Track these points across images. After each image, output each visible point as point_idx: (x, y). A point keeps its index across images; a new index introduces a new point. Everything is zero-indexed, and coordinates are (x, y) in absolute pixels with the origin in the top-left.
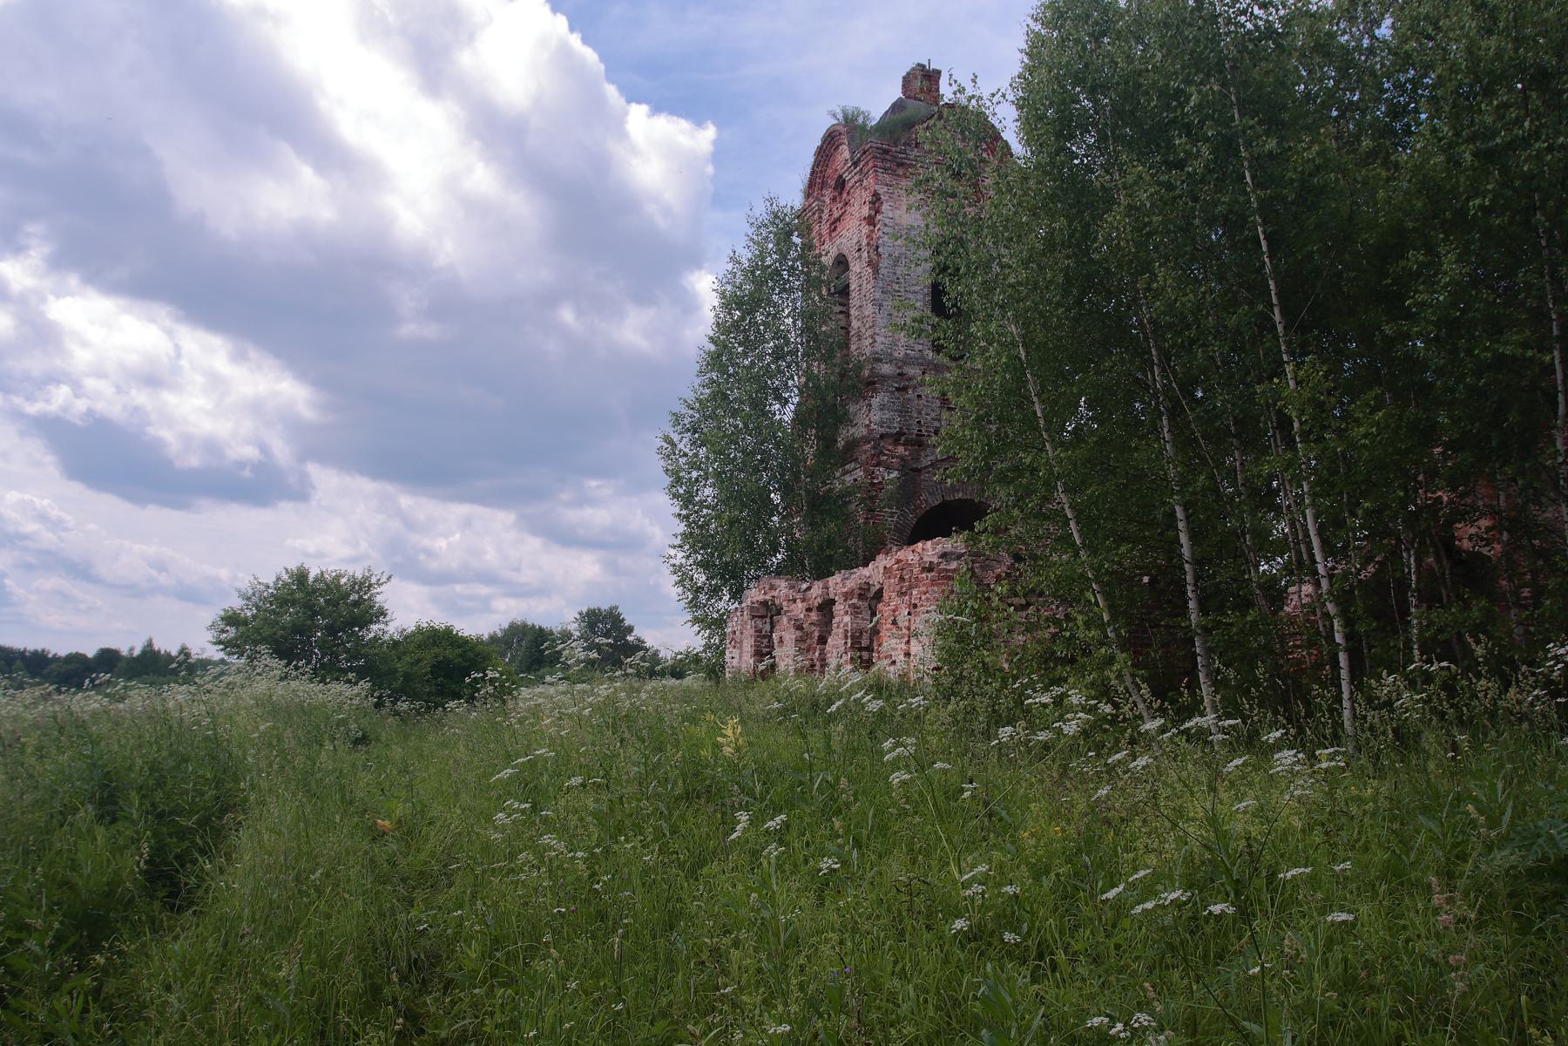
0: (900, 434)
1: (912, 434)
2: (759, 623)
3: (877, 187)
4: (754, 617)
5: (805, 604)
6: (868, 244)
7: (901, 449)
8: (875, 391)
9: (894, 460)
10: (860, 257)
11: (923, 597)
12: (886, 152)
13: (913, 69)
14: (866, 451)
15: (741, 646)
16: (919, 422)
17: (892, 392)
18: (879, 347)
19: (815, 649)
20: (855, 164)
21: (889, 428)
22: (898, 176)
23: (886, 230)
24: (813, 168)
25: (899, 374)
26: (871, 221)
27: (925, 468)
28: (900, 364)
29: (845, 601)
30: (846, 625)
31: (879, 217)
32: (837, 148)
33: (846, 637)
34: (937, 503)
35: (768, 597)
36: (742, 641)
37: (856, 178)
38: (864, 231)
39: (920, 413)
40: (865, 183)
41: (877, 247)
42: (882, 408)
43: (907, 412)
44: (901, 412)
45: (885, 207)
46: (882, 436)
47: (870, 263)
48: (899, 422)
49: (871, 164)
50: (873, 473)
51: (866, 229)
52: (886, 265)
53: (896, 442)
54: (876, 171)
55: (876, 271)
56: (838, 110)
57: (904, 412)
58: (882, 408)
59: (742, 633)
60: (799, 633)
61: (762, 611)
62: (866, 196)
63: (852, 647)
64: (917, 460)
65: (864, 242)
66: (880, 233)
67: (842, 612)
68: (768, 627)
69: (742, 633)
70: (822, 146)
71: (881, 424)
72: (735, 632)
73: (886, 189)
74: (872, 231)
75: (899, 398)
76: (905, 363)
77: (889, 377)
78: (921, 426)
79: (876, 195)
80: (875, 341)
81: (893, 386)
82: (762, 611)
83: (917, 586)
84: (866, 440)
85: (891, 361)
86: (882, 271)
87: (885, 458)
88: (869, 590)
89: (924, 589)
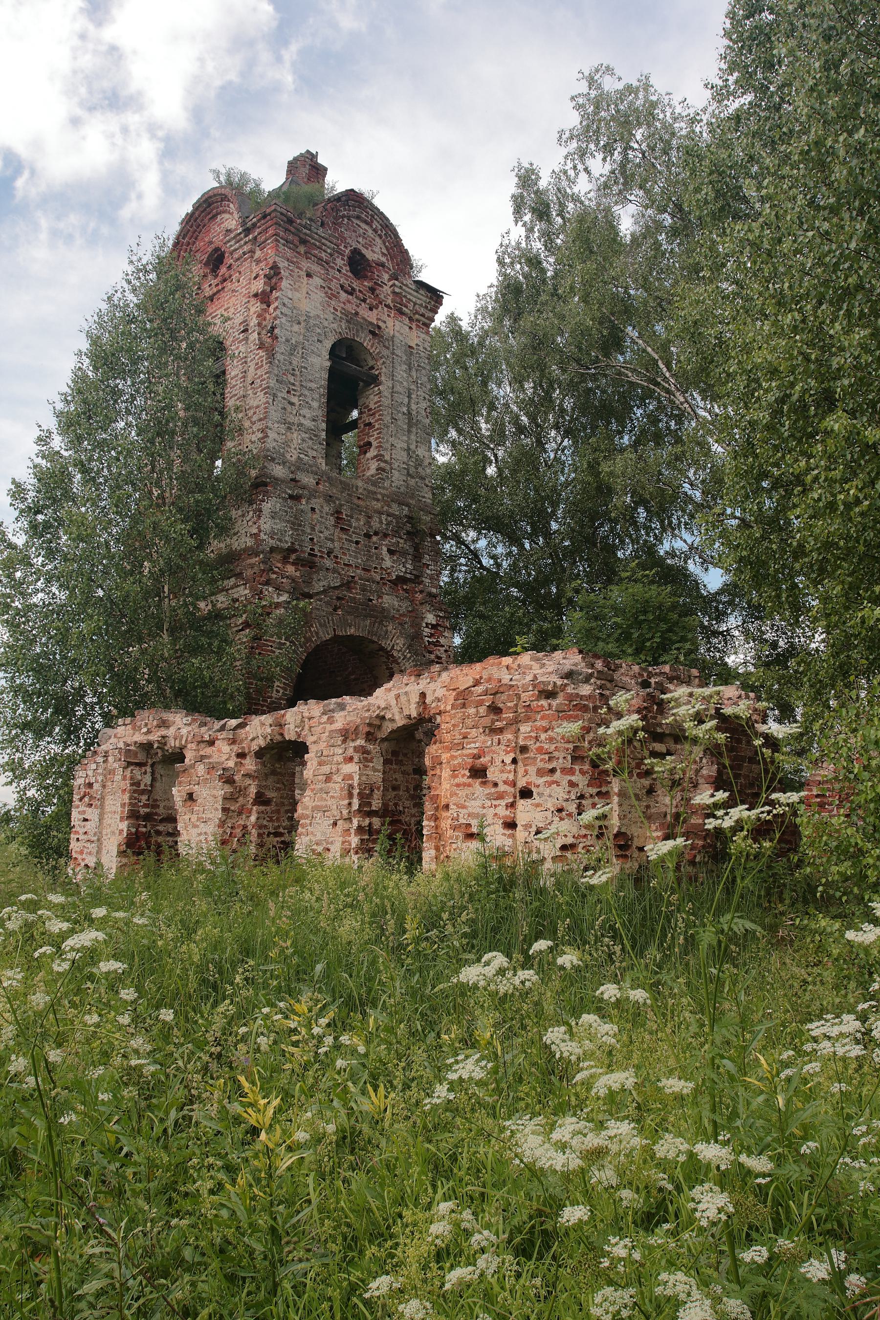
0: (291, 550)
1: (304, 552)
2: (137, 772)
3: (277, 259)
4: (129, 764)
5: (235, 748)
6: (259, 324)
7: (290, 569)
8: (266, 494)
9: (284, 580)
10: (247, 339)
11: (543, 736)
12: (290, 221)
13: (302, 155)
14: (252, 566)
15: (102, 806)
16: (312, 539)
17: (283, 498)
18: (270, 444)
19: (250, 812)
20: (247, 231)
21: (280, 541)
22: (299, 253)
23: (284, 310)
24: (177, 238)
25: (292, 480)
26: (264, 298)
27: (318, 593)
28: (293, 468)
29: (344, 741)
30: (350, 777)
31: (275, 294)
32: (214, 217)
33: (350, 795)
34: (328, 637)
35: (154, 737)
36: (103, 798)
37: (246, 248)
38: (253, 310)
39: (313, 529)
40: (258, 254)
41: (273, 328)
42: (274, 515)
43: (300, 525)
44: (293, 524)
45: (284, 284)
46: (272, 550)
47: (261, 346)
48: (291, 536)
49: (271, 231)
50: (261, 592)
51: (256, 307)
52: (283, 350)
53: (285, 560)
54: (277, 240)
55: (271, 355)
56: (223, 171)
57: (296, 524)
58: (274, 515)
59: (104, 786)
60: (228, 789)
61: (141, 757)
62: (263, 269)
63: (359, 811)
64: (308, 583)
65: (254, 321)
66: (278, 312)
67: (340, 759)
68: (148, 779)
69: (104, 786)
70: (193, 213)
71: (272, 535)
72: (90, 785)
73: (286, 264)
74: (265, 310)
75: (291, 508)
76: (298, 468)
77: (283, 481)
78: (314, 544)
79: (275, 268)
80: (267, 436)
81: (286, 493)
82: (141, 757)
83: (528, 719)
84: (252, 552)
85: (284, 463)
86: (278, 356)
87: (274, 576)
88: (379, 727)
89: (544, 723)
